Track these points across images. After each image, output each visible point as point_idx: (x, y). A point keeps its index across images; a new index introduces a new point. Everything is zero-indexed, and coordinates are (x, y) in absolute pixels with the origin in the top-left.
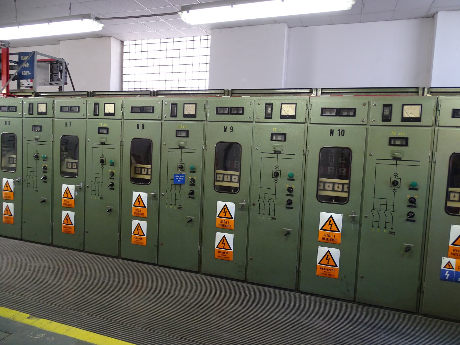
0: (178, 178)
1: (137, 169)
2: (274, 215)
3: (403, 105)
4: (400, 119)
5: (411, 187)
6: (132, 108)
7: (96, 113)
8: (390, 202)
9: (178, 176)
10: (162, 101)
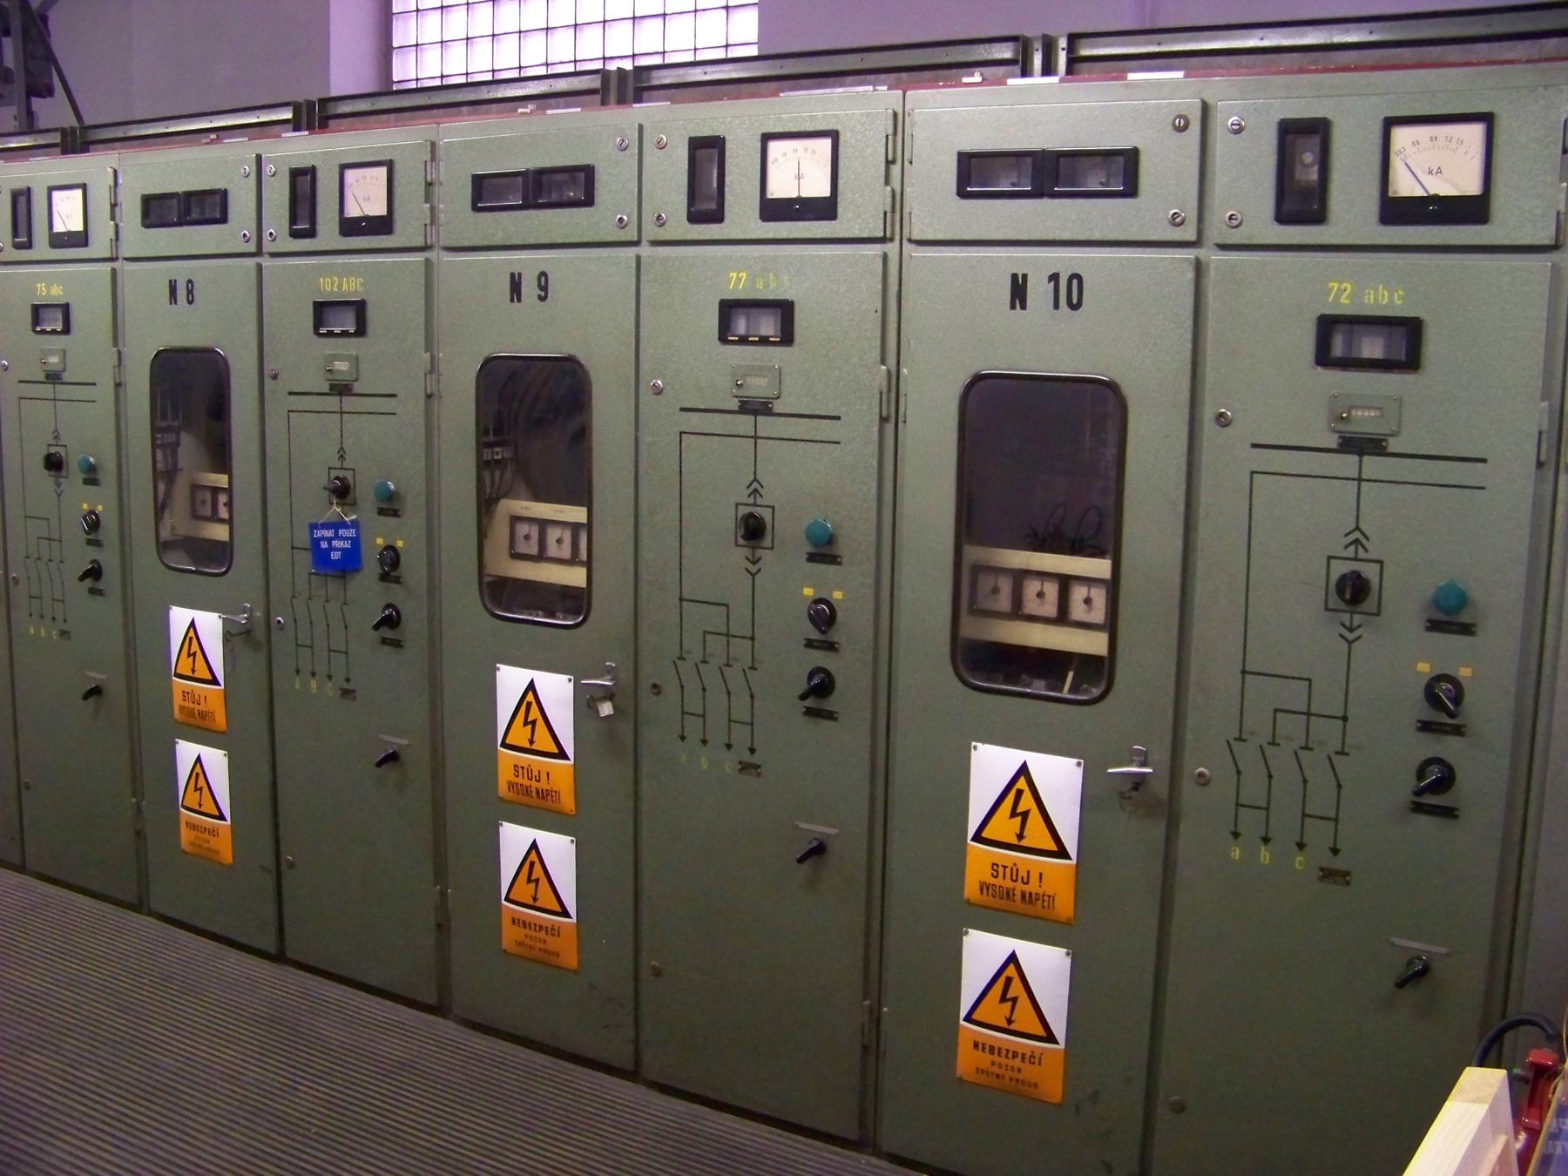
0: (329, 540)
1: (986, 583)
2: (752, 751)
3: (1390, 123)
4: (1372, 206)
5: (1441, 616)
6: (478, 181)
7: (706, 205)
8: (1328, 700)
9: (329, 533)
10: (259, 158)
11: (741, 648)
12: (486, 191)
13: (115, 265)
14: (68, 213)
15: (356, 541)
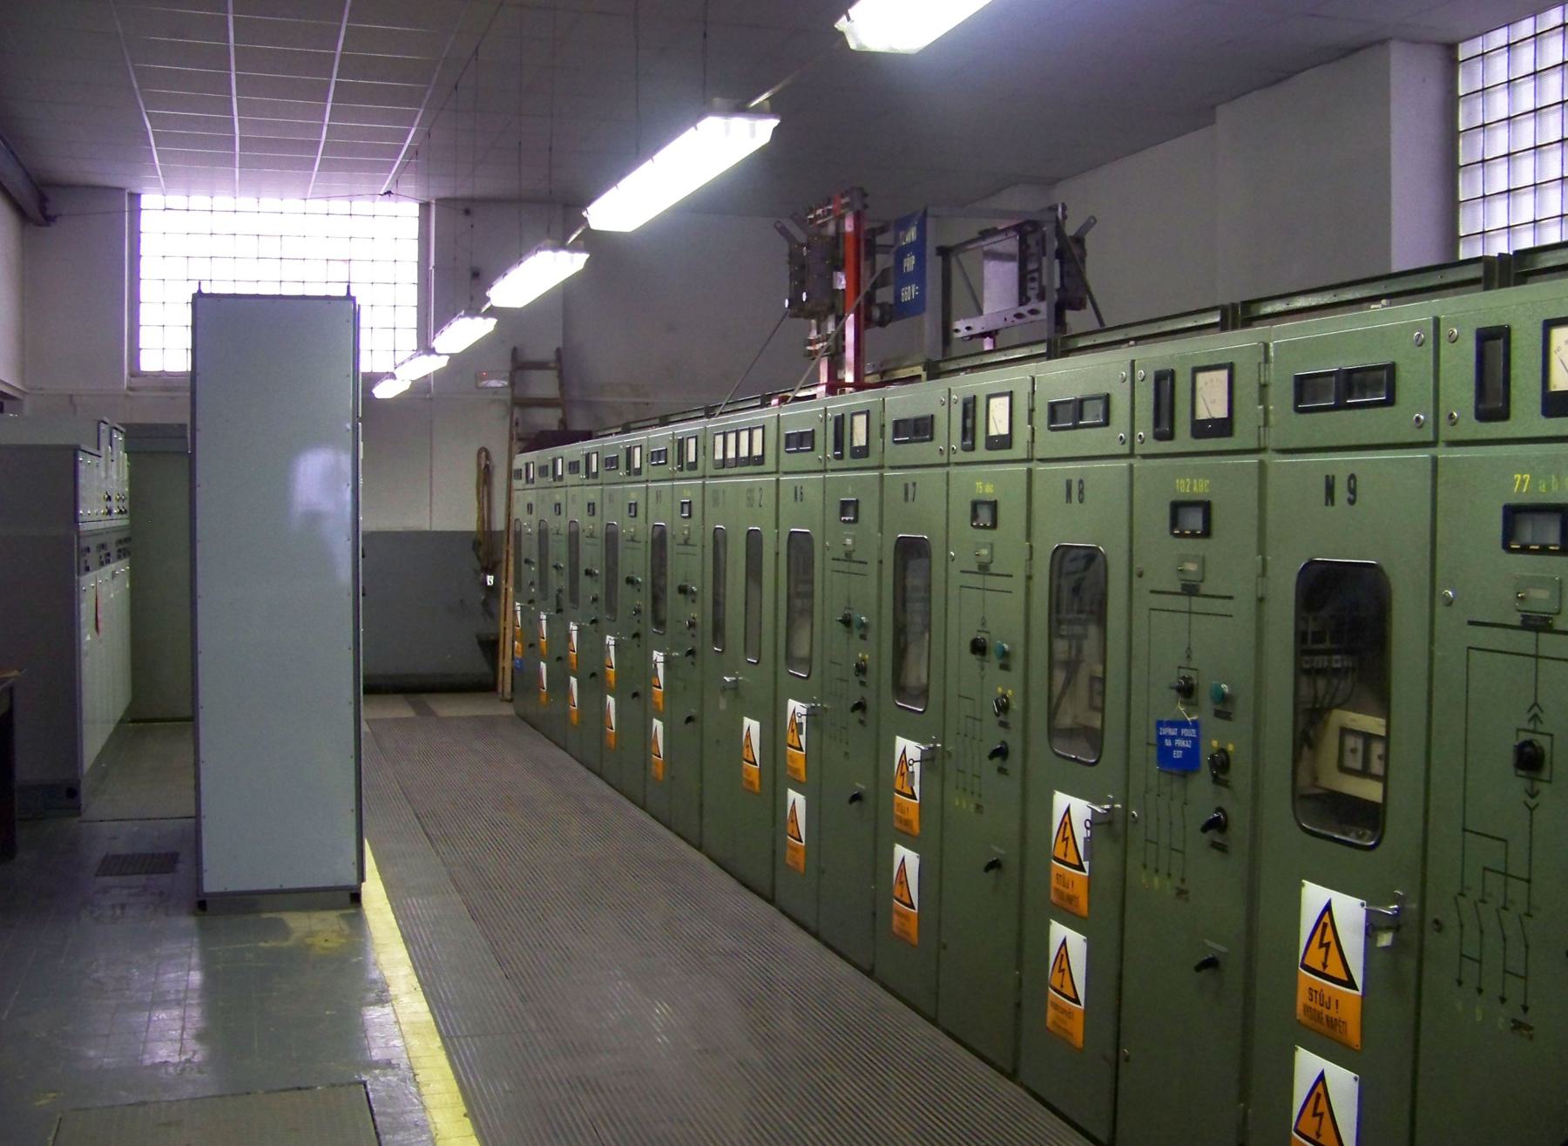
0: (1173, 738)
7: (1492, 400)
9: (1172, 732)
10: (1437, 321)
11: (1517, 889)
12: (1305, 389)
13: (1031, 465)
14: (998, 419)
15: (1195, 741)
